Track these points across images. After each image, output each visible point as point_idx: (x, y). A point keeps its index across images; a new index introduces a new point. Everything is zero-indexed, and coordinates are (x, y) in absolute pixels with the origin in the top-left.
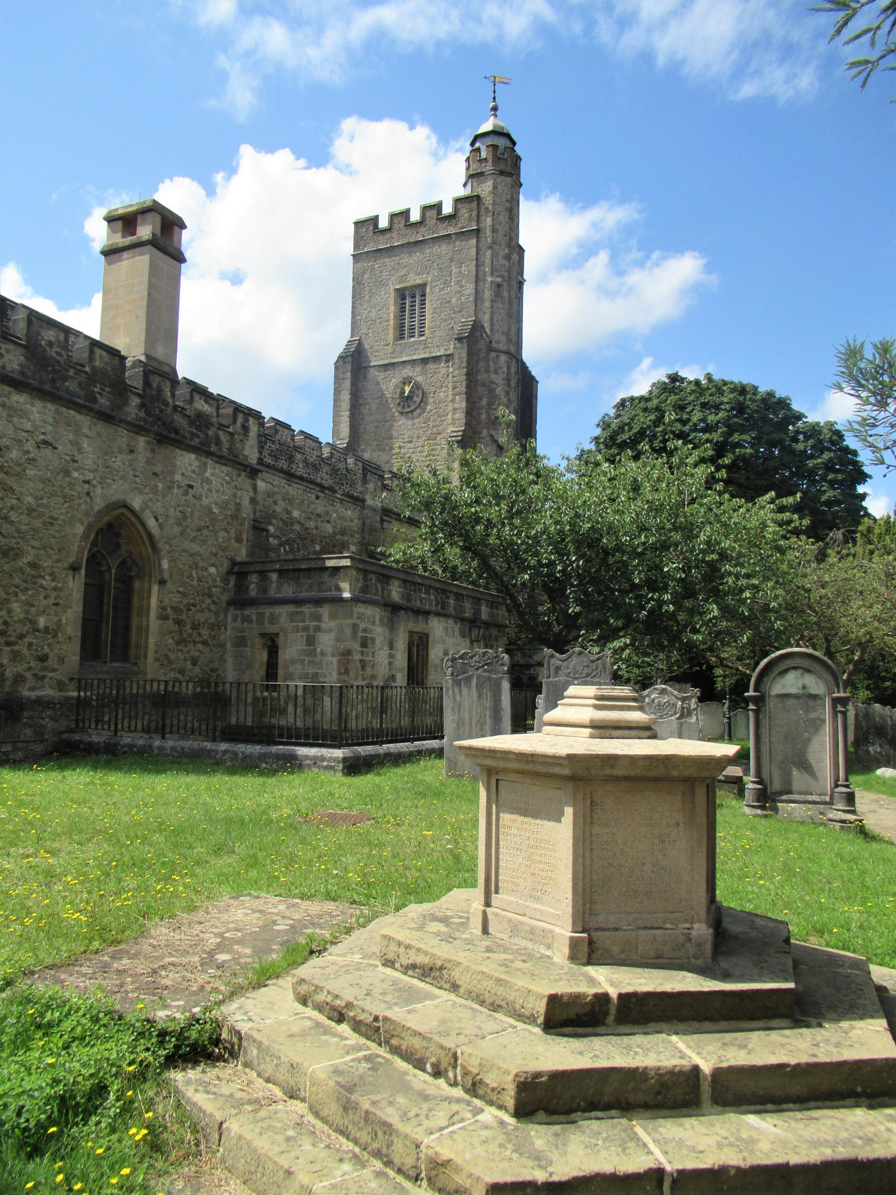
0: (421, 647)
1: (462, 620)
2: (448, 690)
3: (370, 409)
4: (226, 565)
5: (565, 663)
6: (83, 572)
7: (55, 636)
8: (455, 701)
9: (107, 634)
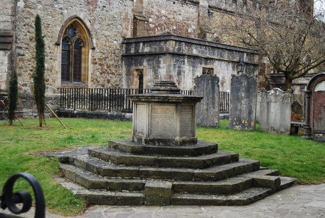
1: (233, 62)
4: (121, 40)
6: (61, 45)
7: (51, 71)
9: (72, 70)
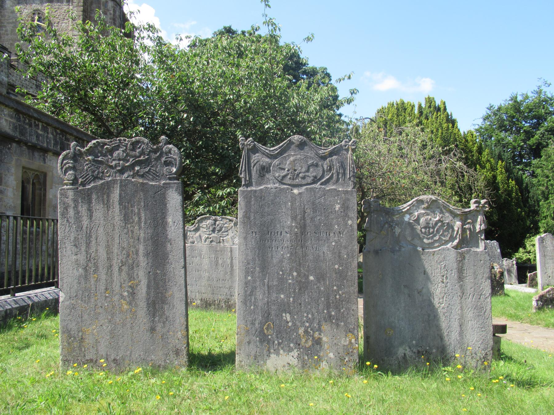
0: (37, 187)
2: (66, 208)
3: (6, 31)
5: (276, 162)
8: (80, 228)
